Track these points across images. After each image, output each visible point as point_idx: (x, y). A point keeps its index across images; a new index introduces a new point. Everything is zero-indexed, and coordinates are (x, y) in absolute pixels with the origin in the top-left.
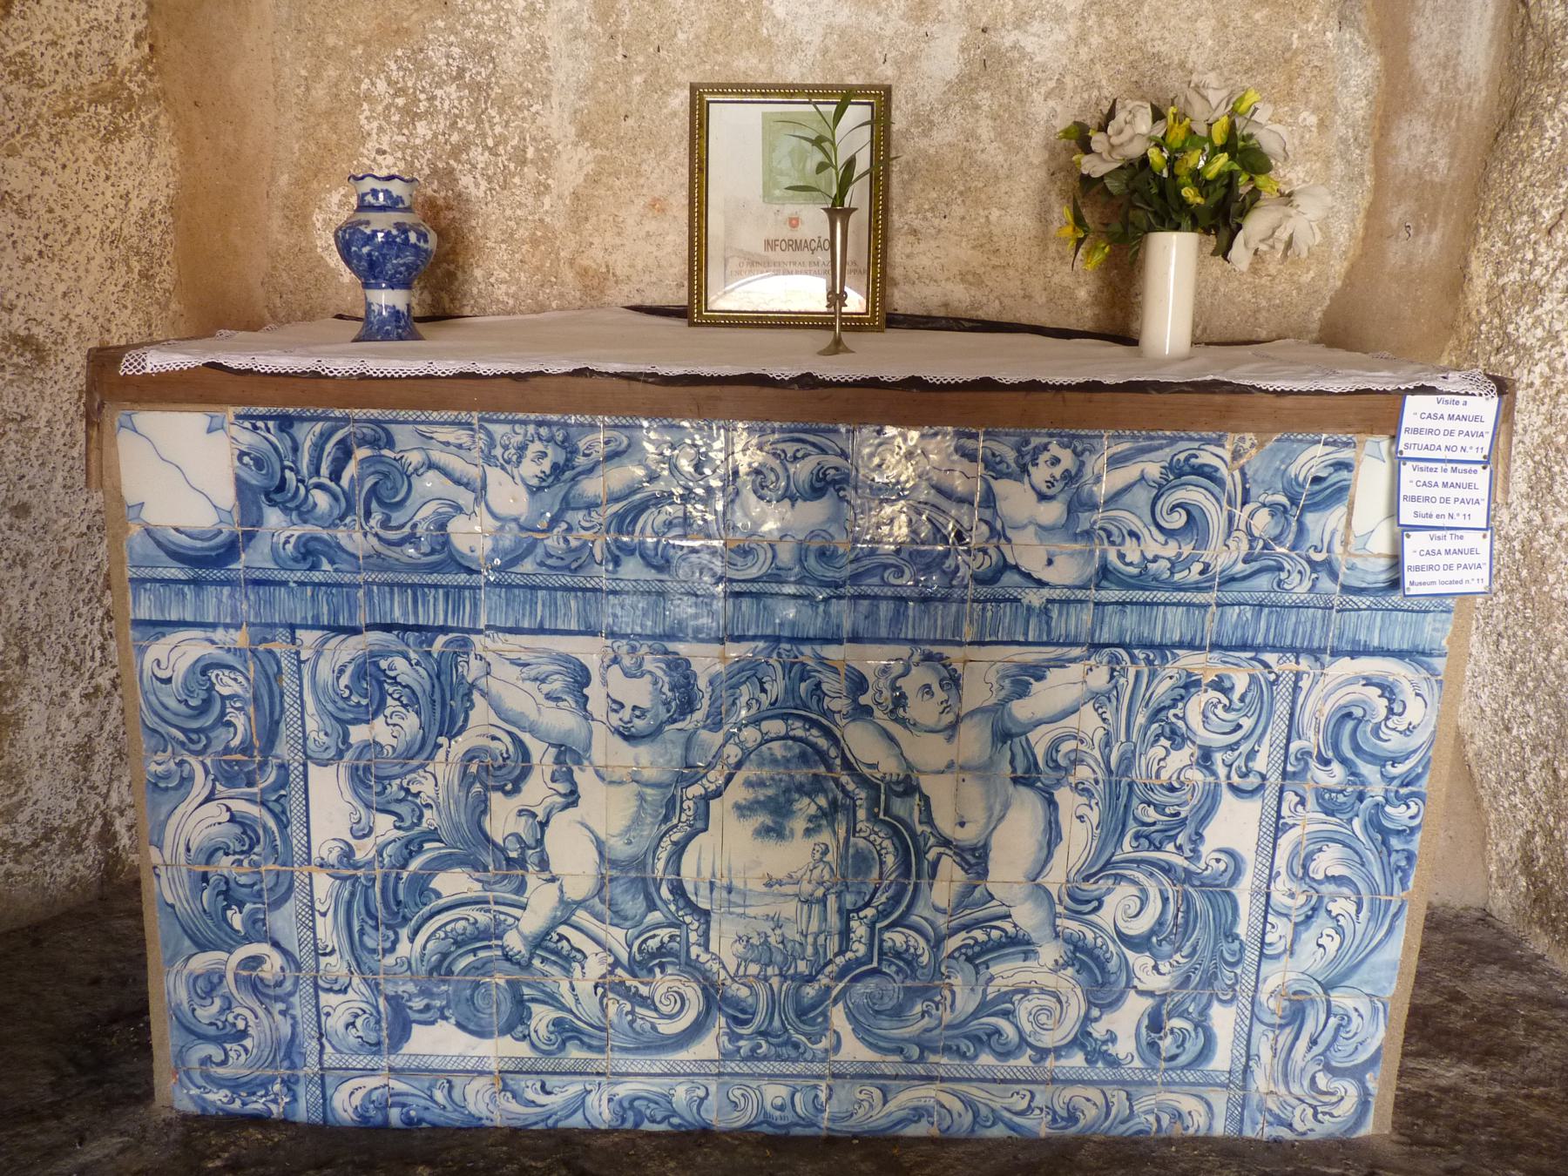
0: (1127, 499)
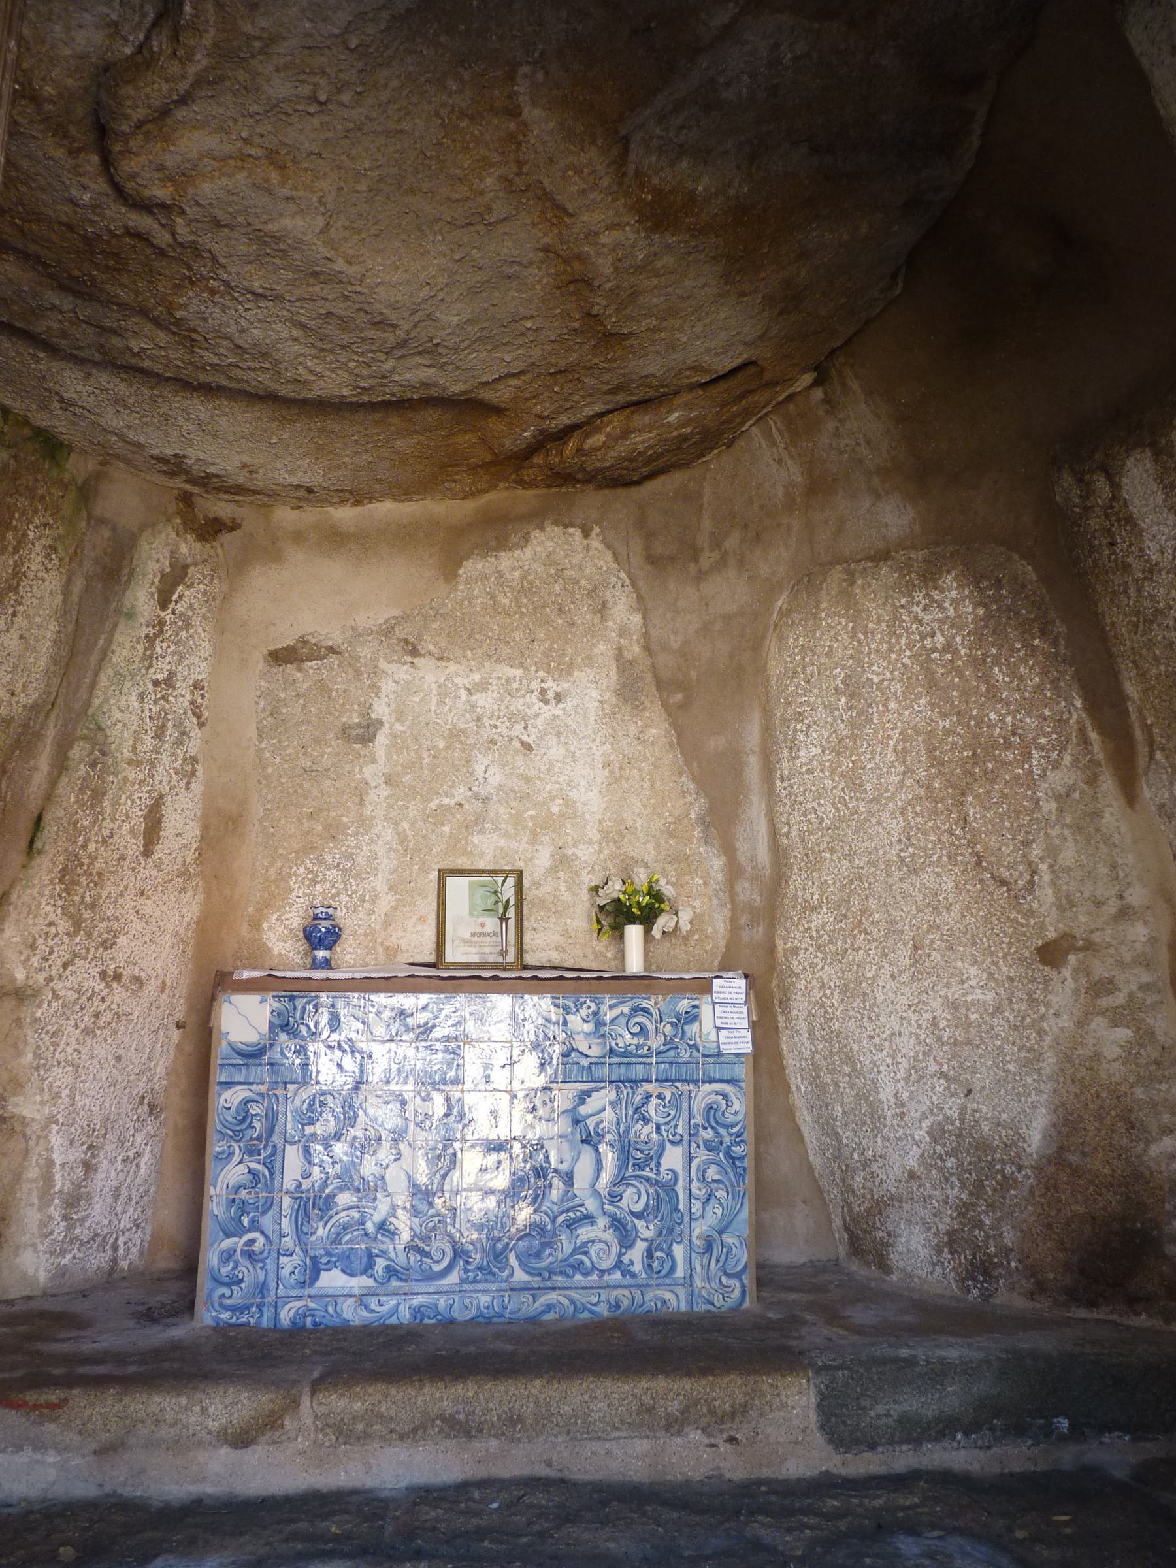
0: (617, 1021)
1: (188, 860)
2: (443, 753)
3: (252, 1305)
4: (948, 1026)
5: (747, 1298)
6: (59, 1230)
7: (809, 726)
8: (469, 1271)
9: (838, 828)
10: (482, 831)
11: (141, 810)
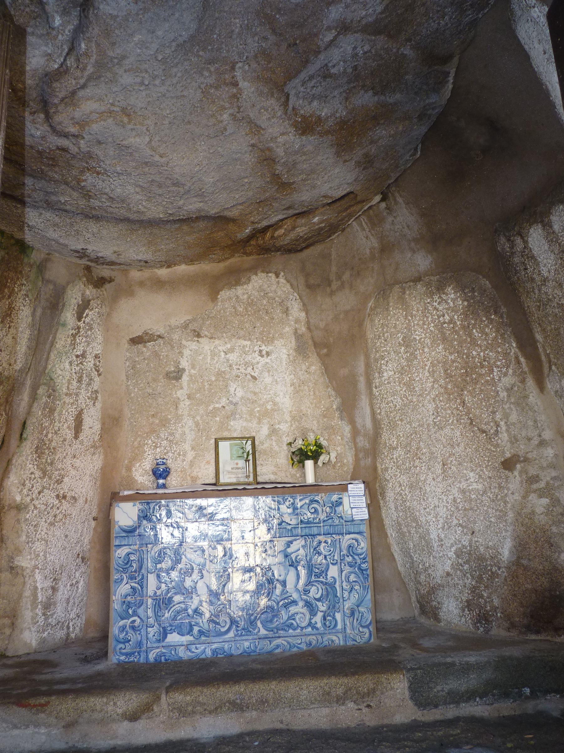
1: (96, 440)
2: (215, 383)
3: (135, 652)
4: (461, 502)
7: (387, 362)
8: (238, 631)
10: (234, 419)
11: (72, 417)
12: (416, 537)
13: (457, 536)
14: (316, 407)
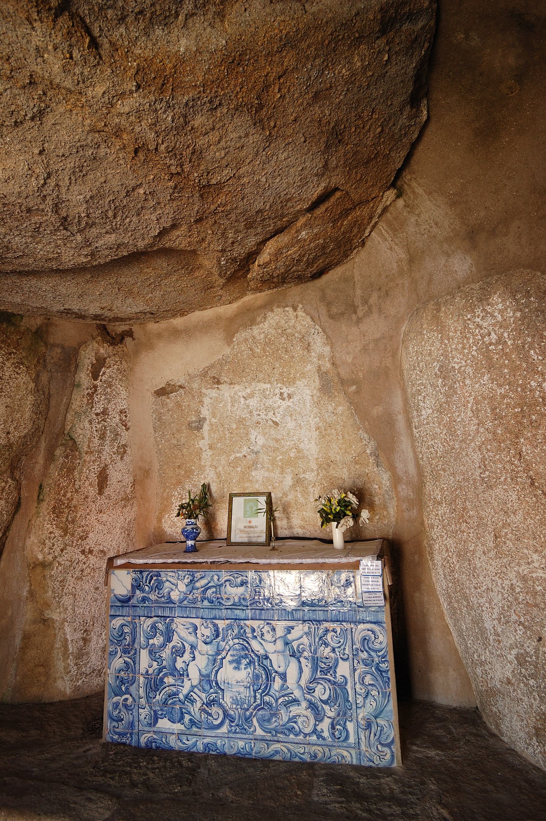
1: (128, 492)
2: (235, 431)
3: (127, 733)
4: (521, 592)
5: (395, 761)
6: (74, 670)
7: (424, 397)
8: (232, 726)
9: (445, 457)
10: (256, 469)
11: (95, 474)
12: (468, 619)
13: (517, 637)
14: (345, 452)
